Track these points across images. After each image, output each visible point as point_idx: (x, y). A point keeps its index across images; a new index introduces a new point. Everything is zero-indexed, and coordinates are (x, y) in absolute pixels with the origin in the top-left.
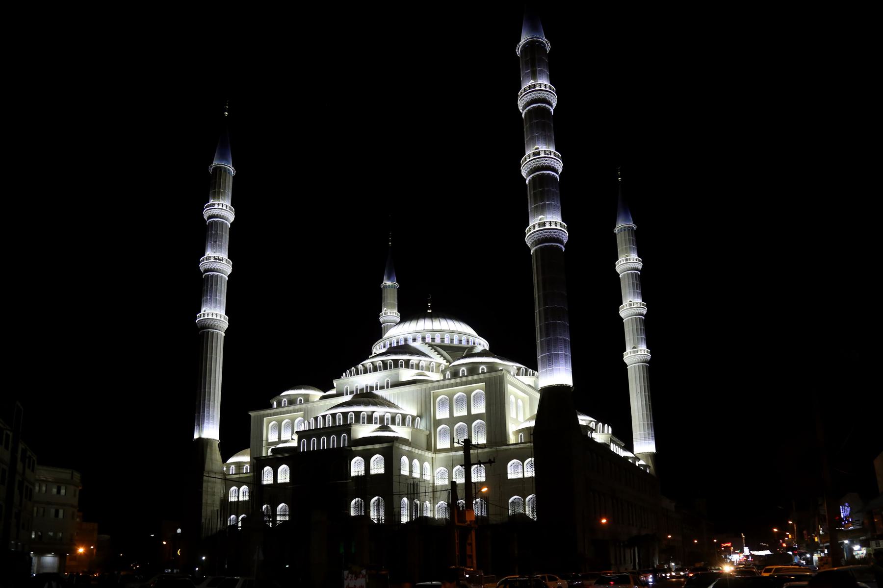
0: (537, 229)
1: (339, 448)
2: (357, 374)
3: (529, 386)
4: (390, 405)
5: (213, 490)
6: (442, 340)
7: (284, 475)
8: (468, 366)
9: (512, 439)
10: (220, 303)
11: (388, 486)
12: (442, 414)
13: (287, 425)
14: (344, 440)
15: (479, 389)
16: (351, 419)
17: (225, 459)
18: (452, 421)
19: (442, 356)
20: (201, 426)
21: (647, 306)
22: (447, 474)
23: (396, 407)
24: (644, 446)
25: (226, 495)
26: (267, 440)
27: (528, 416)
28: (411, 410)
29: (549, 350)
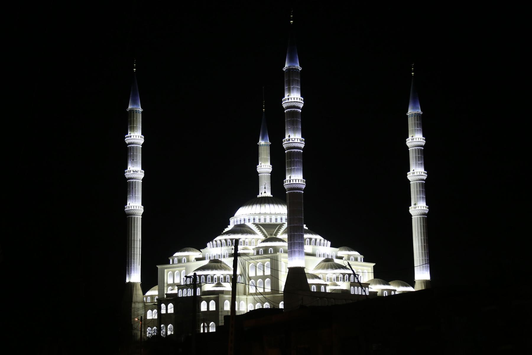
5: (138, 306)
7: (171, 308)
8: (264, 248)
15: (268, 262)
17: (144, 292)
18: (256, 278)
20: (130, 274)
21: (427, 174)
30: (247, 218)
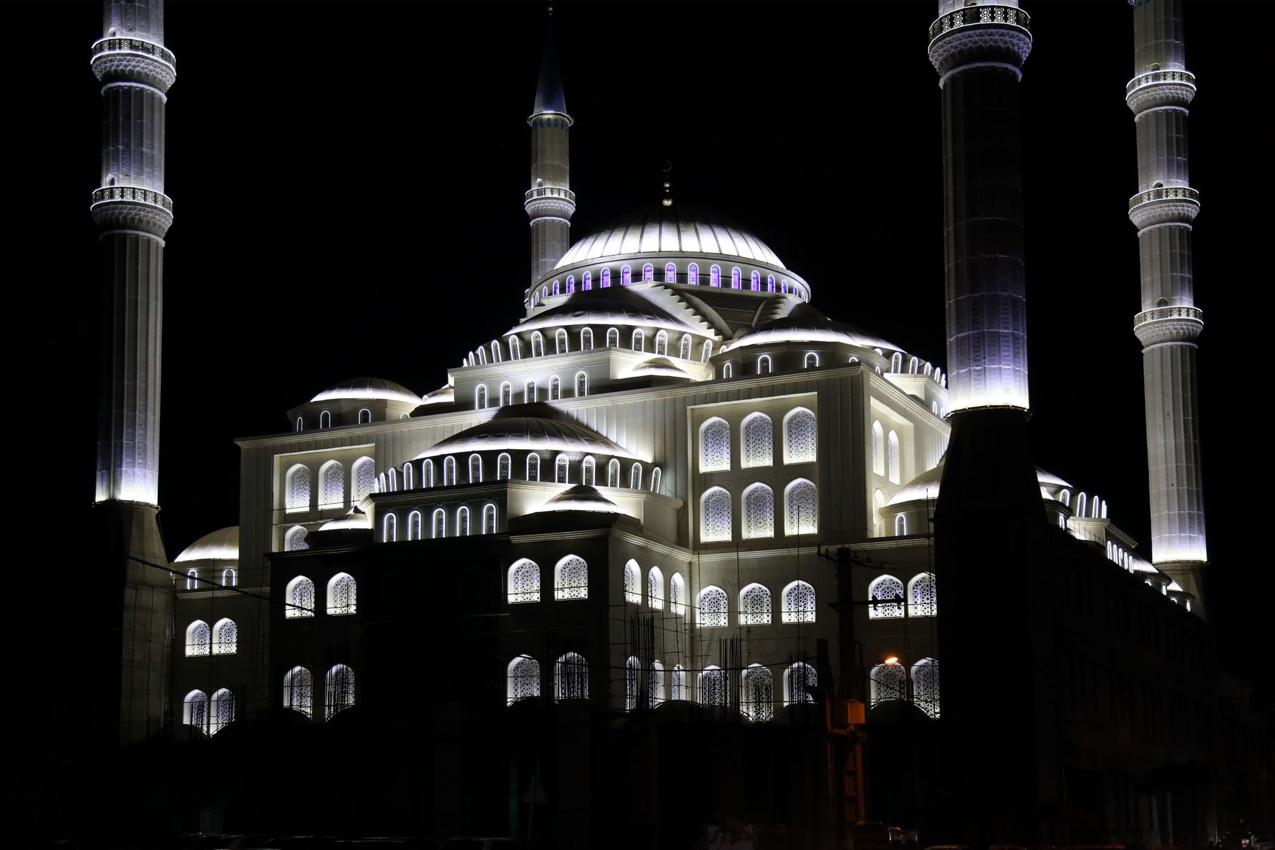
0: (959, 24)
1: (477, 538)
2: (507, 357)
3: (914, 397)
4: (593, 436)
6: (704, 279)
7: (341, 596)
8: (777, 351)
9: (878, 527)
10: (152, 164)
11: (603, 630)
12: (714, 462)
13: (331, 474)
14: (490, 518)
15: (801, 407)
16: (504, 467)
17: (172, 552)
18: (736, 478)
19: (705, 318)
21: (1200, 198)
22: (767, 600)
23: (605, 441)
24: (1179, 547)
25: (179, 642)
26: (282, 508)
27: (912, 475)
28: (638, 449)
29: (975, 323)
30: (627, 267)
